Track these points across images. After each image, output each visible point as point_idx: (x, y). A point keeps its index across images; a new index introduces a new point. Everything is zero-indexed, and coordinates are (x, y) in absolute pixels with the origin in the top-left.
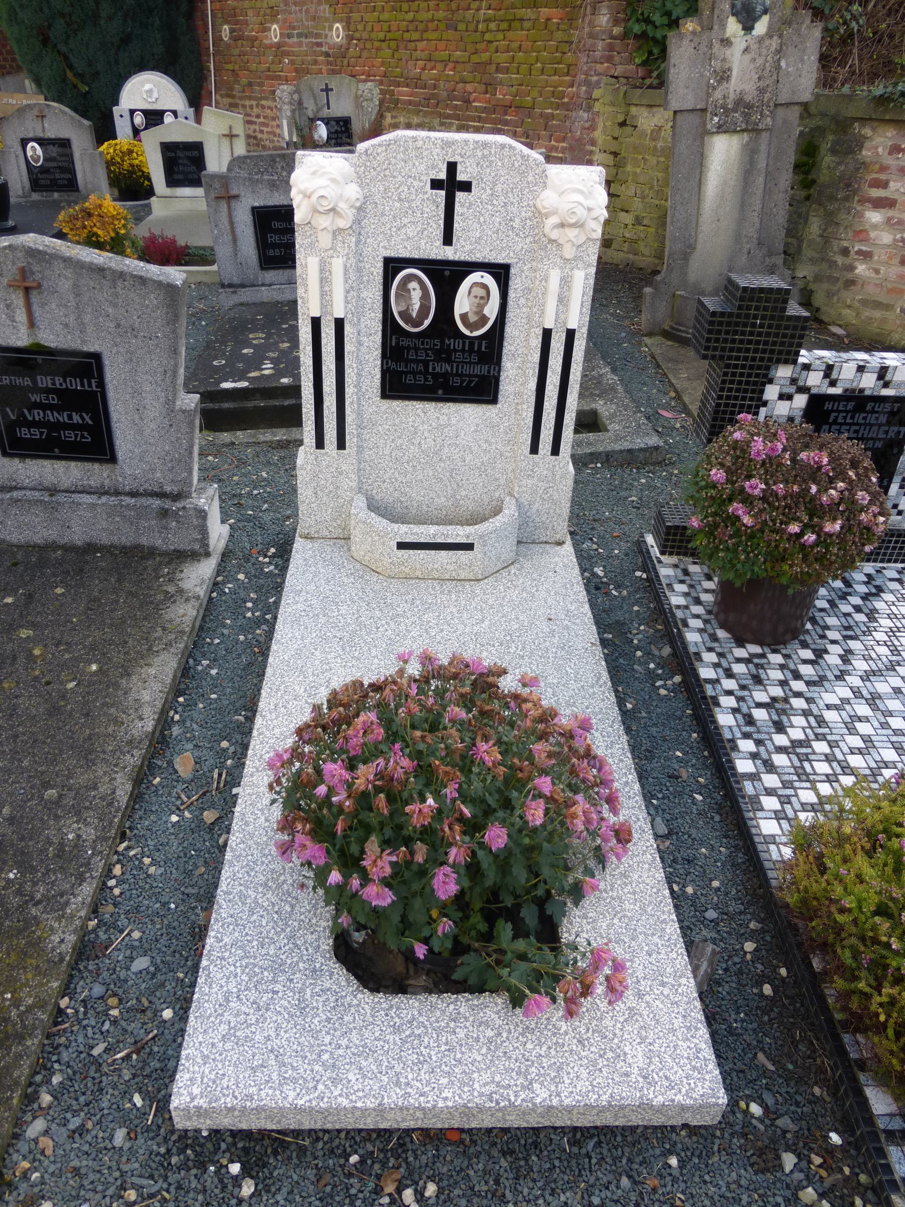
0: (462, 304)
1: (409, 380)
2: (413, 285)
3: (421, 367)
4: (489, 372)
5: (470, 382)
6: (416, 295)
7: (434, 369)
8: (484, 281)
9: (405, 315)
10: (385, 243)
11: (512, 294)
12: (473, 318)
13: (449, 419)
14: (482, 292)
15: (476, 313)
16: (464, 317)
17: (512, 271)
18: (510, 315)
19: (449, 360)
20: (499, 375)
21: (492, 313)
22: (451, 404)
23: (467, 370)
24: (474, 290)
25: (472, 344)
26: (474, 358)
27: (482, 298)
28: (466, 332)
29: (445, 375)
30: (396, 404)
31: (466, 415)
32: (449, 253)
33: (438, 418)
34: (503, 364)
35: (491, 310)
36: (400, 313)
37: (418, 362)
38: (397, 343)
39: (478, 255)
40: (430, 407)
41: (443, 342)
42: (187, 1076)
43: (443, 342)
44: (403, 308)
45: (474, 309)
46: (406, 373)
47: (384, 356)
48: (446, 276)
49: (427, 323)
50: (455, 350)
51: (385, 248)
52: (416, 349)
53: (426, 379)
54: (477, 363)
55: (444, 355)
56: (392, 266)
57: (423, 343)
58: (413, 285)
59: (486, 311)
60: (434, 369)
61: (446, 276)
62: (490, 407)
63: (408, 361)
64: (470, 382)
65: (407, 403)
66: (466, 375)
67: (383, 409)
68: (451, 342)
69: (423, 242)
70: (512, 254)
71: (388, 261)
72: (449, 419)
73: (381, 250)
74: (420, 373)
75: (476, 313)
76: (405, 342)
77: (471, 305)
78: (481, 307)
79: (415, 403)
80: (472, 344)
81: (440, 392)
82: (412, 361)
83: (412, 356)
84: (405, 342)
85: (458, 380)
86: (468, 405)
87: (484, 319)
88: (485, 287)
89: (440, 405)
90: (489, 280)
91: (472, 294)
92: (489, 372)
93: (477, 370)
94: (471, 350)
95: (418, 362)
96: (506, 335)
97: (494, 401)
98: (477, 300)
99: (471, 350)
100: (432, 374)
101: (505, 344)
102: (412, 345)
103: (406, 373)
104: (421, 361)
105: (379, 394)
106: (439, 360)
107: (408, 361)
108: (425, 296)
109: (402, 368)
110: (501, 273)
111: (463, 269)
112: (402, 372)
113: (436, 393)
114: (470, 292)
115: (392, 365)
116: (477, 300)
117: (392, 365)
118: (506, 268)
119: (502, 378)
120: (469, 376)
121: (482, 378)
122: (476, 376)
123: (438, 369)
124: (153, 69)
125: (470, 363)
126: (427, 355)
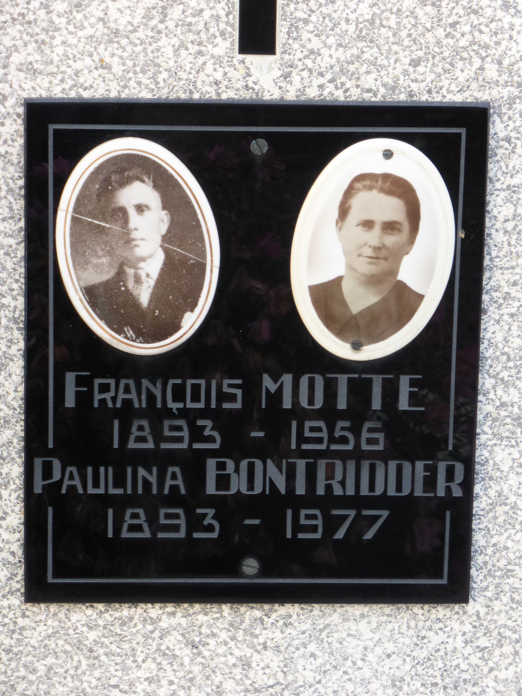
0: (320, 248)
1: (133, 526)
2: (138, 193)
3: (176, 479)
4: (430, 483)
5: (361, 523)
6: (148, 228)
7: (223, 481)
8: (395, 167)
9: (111, 299)
10: (29, 54)
11: (499, 208)
12: (359, 299)
13: (287, 664)
14: (391, 208)
15: (373, 281)
16: (327, 297)
17: (497, 128)
18: (498, 279)
19: (272, 448)
20: (468, 496)
21: (429, 276)
22: (292, 610)
23: (344, 479)
24: (356, 202)
25: (360, 390)
26: (372, 438)
27: (390, 227)
28: (338, 347)
29: (272, 505)
30: (83, 618)
31: (353, 648)
32: (265, 80)
33: (246, 664)
34: (481, 454)
35: (428, 268)
36: (91, 293)
37: (161, 460)
38: (84, 398)
39: (368, 81)
40: (215, 623)
41: (251, 388)
42: (330, 88)
43: (251, 388)
44: (100, 273)
45: (365, 267)
46: (121, 504)
47: (34, 445)
48: (256, 162)
49: (191, 322)
50: (299, 413)
51: (30, 70)
52: (156, 415)
53: (195, 523)
54: (384, 457)
55: (258, 431)
56: (57, 132)
57: (179, 394)
58: (138, 193)
59: (409, 273)
60: (223, 481)
61: (256, 162)
62: (441, 611)
63: (124, 461)
64: (361, 523)
65: (125, 611)
66: (345, 502)
67: (34, 638)
68: (288, 389)
69: (167, 45)
70: (491, 71)
71: (39, 116)
72: (287, 664)
73: (15, 76)
74: (174, 499)
75: (373, 281)
76: (111, 393)
77: (352, 253)
78: (388, 258)
79: (154, 610)
80: (360, 390)
81: (251, 566)
82: (143, 459)
83: (140, 438)
84: (111, 393)
85: (312, 518)
86: (356, 610)
87: (404, 301)
88: (402, 190)
89: (251, 613)
90: (413, 164)
91: (356, 215)
92: (430, 483)
93: (386, 480)
94: (359, 411)
95: (161, 460)
96: (486, 350)
97: (455, 589)
98: (374, 237)
99: (359, 411)
100: (212, 502)
101: (485, 382)
102: (140, 403)
103: (121, 504)
104: (172, 458)
105: (18, 584)
106: (236, 446)
107: (124, 461)
108: (182, 229)
109: (102, 483)
110: (456, 138)
111: (314, 133)
112: (106, 500)
113: (235, 570)
114: (344, 211)
115: (69, 478)
116: (374, 237)
117: (69, 478)
118: (474, 120)
119: (479, 505)
120: (357, 501)
121: (402, 508)
122: (383, 501)
123: (238, 484)
124: (301, 376)
125: (358, 455)
126: (197, 434)
